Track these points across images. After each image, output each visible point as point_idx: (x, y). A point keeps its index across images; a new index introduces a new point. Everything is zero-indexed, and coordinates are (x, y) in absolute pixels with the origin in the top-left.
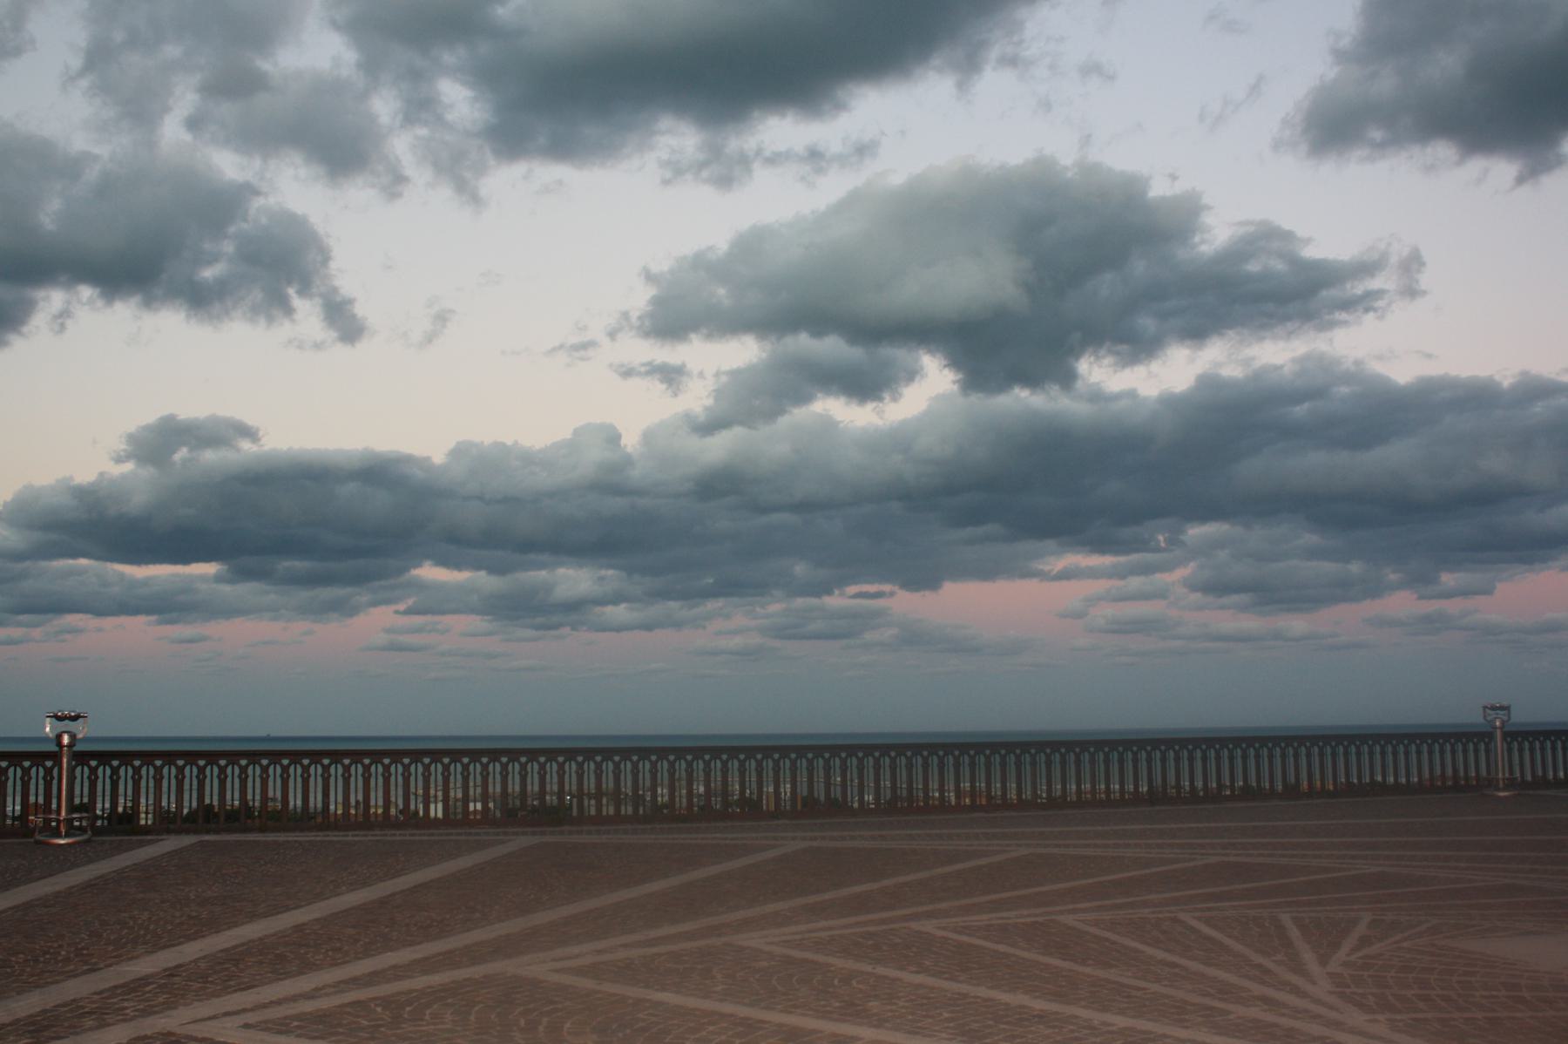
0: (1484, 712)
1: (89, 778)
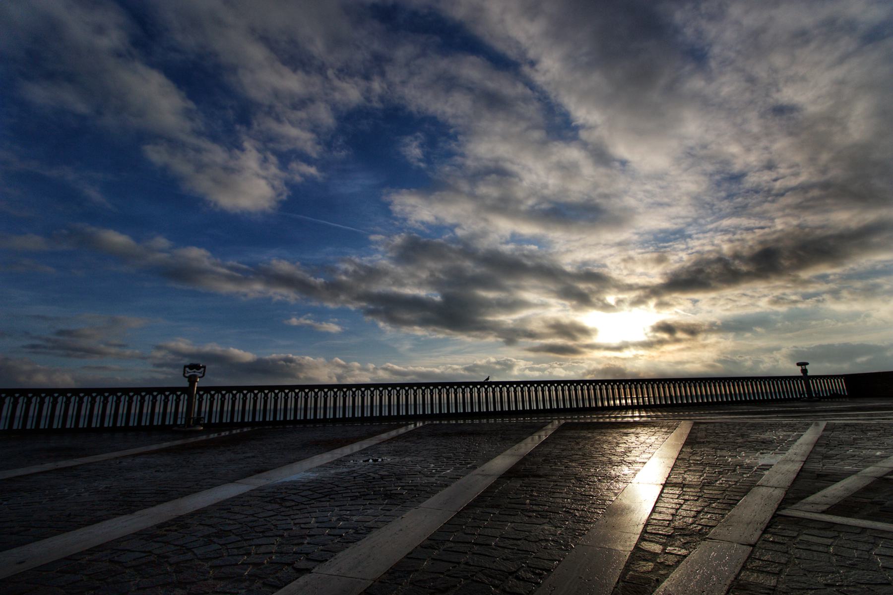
0: (184, 370)
1: (254, 398)
